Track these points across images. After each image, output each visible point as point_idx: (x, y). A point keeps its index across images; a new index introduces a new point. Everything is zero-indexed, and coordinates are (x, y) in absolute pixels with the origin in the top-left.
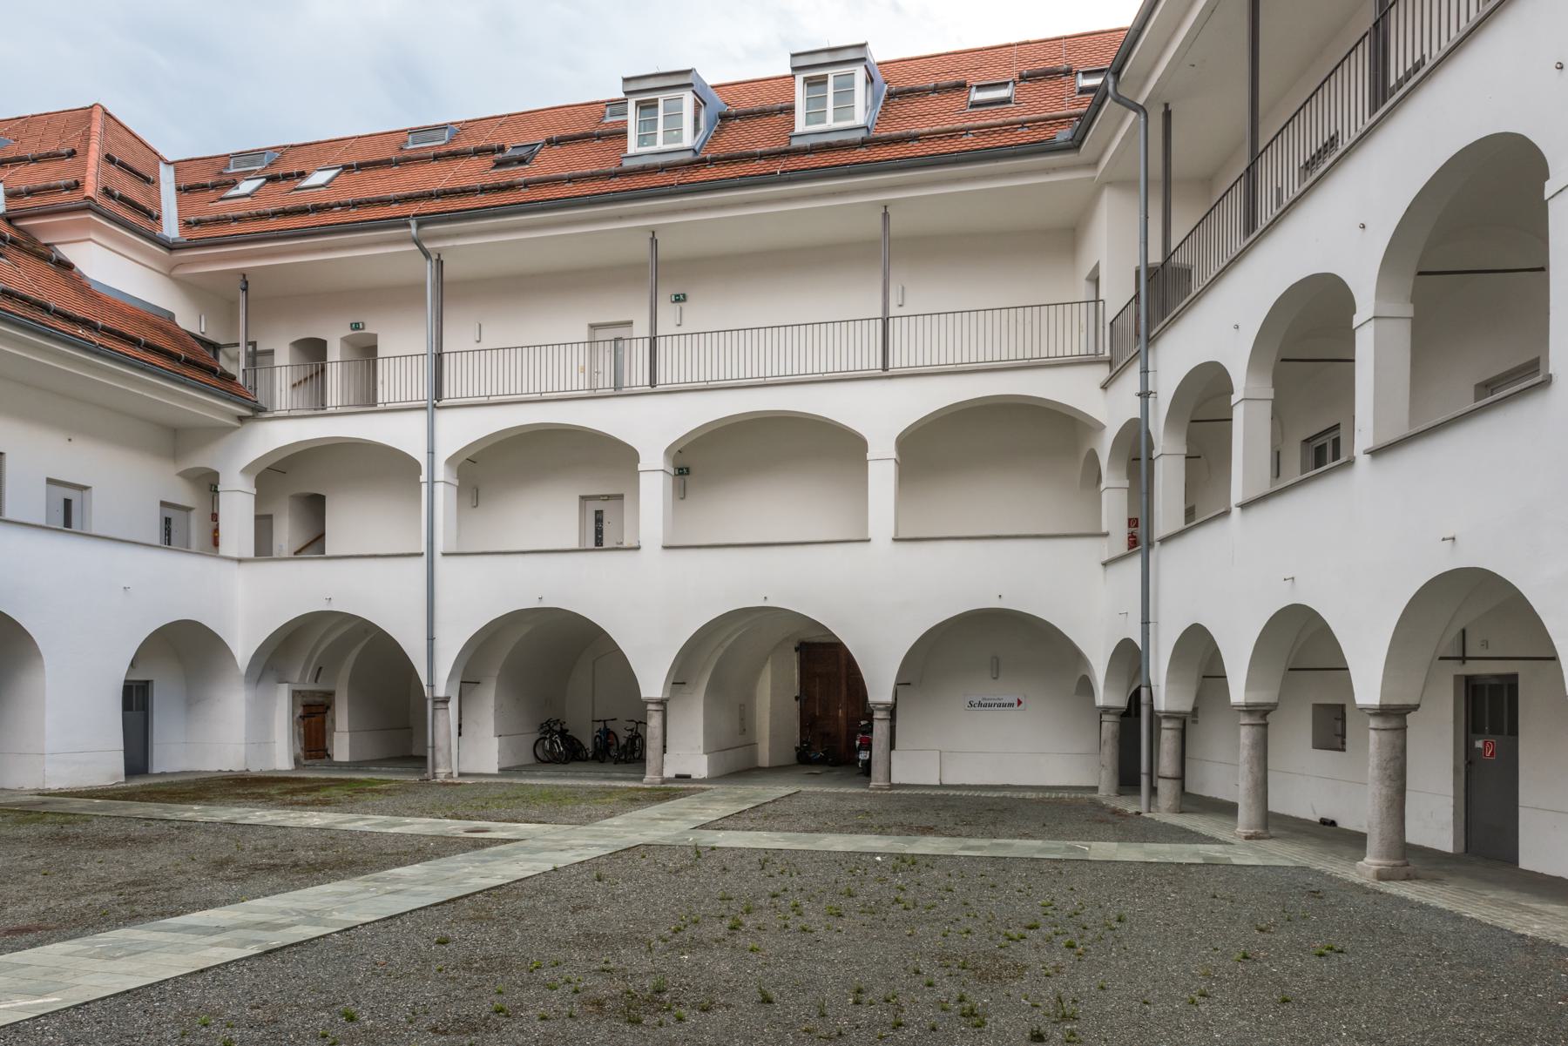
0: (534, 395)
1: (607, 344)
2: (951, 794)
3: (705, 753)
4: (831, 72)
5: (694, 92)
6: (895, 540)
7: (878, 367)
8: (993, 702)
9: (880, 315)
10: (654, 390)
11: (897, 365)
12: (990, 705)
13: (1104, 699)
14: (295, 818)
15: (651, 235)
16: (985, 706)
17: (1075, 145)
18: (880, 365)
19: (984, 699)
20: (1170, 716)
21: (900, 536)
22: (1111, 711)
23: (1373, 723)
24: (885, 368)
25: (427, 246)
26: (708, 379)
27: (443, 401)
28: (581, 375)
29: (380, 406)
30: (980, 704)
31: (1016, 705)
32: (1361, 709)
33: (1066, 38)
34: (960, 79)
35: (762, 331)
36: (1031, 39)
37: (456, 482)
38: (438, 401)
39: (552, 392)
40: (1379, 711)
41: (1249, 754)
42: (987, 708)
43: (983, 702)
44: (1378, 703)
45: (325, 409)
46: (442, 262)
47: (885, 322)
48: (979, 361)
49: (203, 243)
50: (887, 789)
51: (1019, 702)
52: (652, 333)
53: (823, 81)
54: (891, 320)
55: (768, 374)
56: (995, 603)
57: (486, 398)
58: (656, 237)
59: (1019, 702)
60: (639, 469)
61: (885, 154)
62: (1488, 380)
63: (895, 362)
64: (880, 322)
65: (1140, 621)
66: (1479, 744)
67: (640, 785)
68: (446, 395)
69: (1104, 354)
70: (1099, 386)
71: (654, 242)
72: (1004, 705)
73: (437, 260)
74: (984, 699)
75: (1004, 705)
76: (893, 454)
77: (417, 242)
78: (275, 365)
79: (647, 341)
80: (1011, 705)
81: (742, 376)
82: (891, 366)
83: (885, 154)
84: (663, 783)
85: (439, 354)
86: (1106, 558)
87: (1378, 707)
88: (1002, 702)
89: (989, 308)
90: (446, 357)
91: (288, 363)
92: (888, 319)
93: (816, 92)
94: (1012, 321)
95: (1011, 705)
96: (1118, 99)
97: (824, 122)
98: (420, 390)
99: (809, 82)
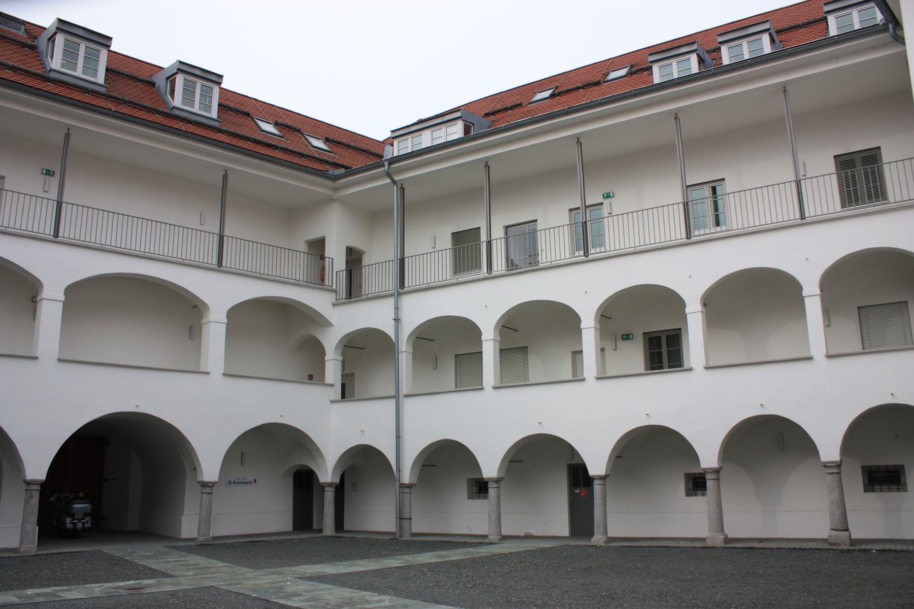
0: (502, 272)
1: (788, 185)
5: (462, 120)
6: (706, 368)
7: (797, 218)
8: (241, 481)
9: (793, 178)
10: (690, 241)
11: (812, 214)
12: (240, 483)
13: (332, 477)
15: (577, 140)
17: (335, 178)
18: (798, 216)
19: (236, 479)
20: (330, 485)
21: (711, 364)
24: (803, 217)
25: (396, 178)
27: (540, 265)
29: (363, 297)
30: (234, 482)
31: (253, 482)
35: (671, 207)
37: (411, 350)
38: (402, 289)
39: (408, 287)
42: (249, 485)
43: (236, 481)
45: (537, 265)
46: (489, 167)
47: (798, 183)
48: (756, 225)
50: (211, 541)
51: (255, 481)
52: (684, 199)
54: (802, 182)
55: (553, 259)
56: (889, 400)
57: (427, 285)
58: (488, 164)
59: (255, 481)
60: (804, 295)
63: (809, 212)
64: (794, 184)
66: (577, 491)
67: (589, 544)
68: (406, 285)
69: (332, 286)
70: (39, 357)
71: (402, 190)
73: (401, 188)
74: (236, 479)
75: (247, 483)
77: (389, 175)
78: (835, 174)
79: (681, 206)
80: (251, 483)
81: (663, 240)
82: (807, 215)
84: (606, 542)
85: (402, 259)
90: (406, 260)
91: (568, 223)
92: (800, 181)
94: (640, 218)
95: (251, 483)
98: (391, 284)
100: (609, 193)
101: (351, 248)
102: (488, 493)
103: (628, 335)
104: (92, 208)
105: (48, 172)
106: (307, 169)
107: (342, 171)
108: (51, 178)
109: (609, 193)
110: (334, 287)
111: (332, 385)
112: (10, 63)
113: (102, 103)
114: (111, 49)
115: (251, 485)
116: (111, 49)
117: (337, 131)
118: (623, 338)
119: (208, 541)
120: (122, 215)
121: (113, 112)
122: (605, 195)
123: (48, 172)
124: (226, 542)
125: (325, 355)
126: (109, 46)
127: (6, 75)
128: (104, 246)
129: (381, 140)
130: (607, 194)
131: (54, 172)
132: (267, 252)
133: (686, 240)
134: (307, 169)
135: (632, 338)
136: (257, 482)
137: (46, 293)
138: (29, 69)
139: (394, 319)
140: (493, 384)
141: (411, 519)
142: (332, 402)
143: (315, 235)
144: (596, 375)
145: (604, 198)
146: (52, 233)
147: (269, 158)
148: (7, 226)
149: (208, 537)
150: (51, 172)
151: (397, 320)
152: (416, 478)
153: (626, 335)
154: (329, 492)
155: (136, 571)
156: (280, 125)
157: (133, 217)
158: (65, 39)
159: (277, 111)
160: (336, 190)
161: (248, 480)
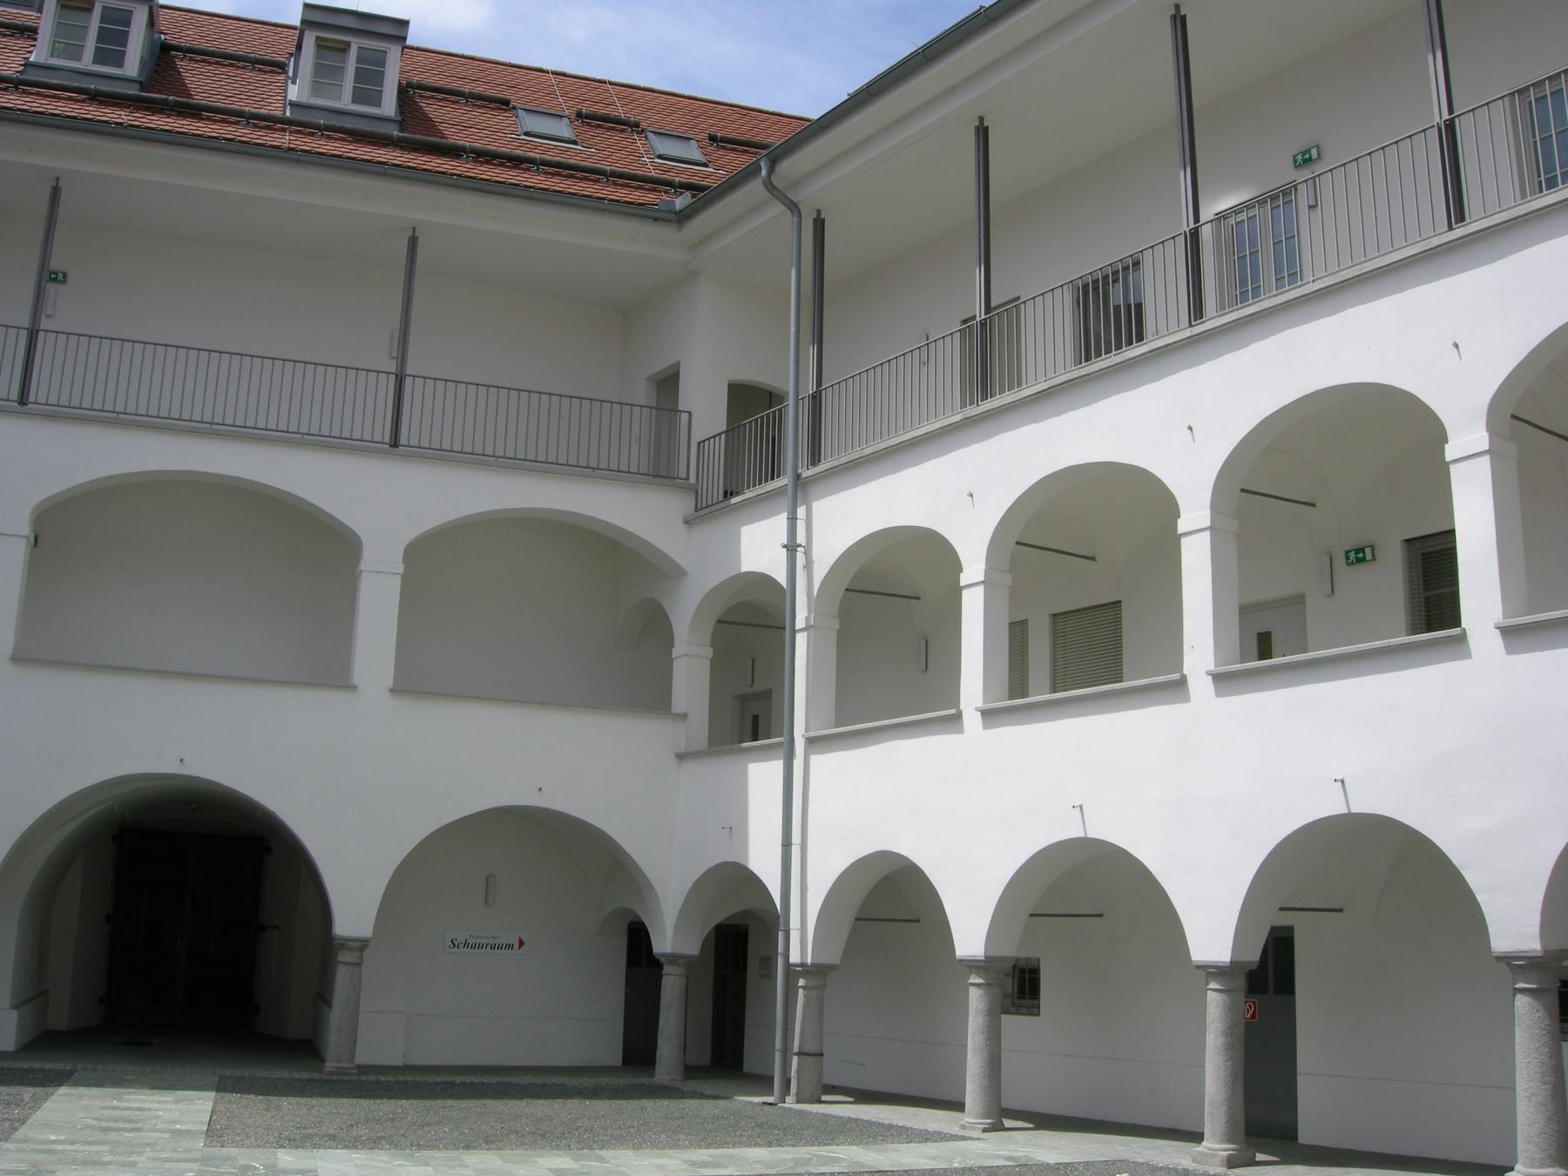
2: (458, 1081)
3: (15, 1007)
4: (356, 43)
8: (485, 941)
12: (481, 946)
14: (170, 1111)
16: (474, 946)
17: (683, 217)
20: (674, 959)
22: (680, 961)
23: (974, 979)
26: (119, 408)
28: (635, 448)
30: (466, 944)
32: (1198, 967)
33: (611, 83)
34: (505, 95)
36: (784, 112)
40: (983, 964)
41: (984, 1022)
43: (471, 941)
44: (1228, 959)
49: (6, 115)
50: (354, 1074)
51: (521, 943)
53: (344, 48)
56: (1330, 805)
59: (521, 943)
61: (19, 102)
62: (434, 528)
65: (780, 843)
69: (688, 479)
72: (500, 947)
75: (500, 947)
76: (401, 569)
80: (510, 946)
82: (32, 398)
83: (19, 102)
86: (682, 749)
87: (1229, 964)
88: (497, 942)
89: (567, 394)
91: (654, 405)
93: (331, 60)
95: (510, 946)
96: (769, 185)
97: (79, 59)
99: (321, 45)
100: (1309, 151)
101: (771, 393)
102: (1038, 999)
103: (1362, 550)
104: (474, 384)
105: (53, 276)
106: (601, 206)
107: (682, 201)
108: (60, 287)
109: (1309, 151)
110: (692, 480)
111: (684, 716)
112: (468, 144)
113: (285, 139)
114: (408, 42)
115: (509, 951)
116: (408, 42)
117: (702, 106)
118: (1348, 558)
119: (347, 1074)
120: (589, 402)
121: (125, 127)
122: (1300, 157)
123: (53, 276)
124: (419, 1079)
125: (672, 644)
126: (405, 39)
127: (576, 187)
128: (120, 416)
129: (815, 116)
130: (1304, 153)
131: (65, 275)
132: (471, 403)
133: (16, 404)
134: (601, 206)
135: (1374, 558)
136: (524, 947)
137: (370, 559)
138: (556, 158)
139: (785, 546)
140: (980, 703)
141: (822, 1055)
142: (681, 757)
143: (660, 365)
144: (1211, 667)
145: (1297, 166)
146: (387, 439)
147: (503, 189)
148: (596, 466)
149: (347, 1065)
150: (60, 276)
151: (791, 548)
152: (840, 945)
153: (1357, 551)
154: (672, 978)
155: (218, 1126)
156: (588, 117)
157: (357, 369)
158: (359, 47)
159: (607, 91)
160: (696, 246)
161: (503, 940)
